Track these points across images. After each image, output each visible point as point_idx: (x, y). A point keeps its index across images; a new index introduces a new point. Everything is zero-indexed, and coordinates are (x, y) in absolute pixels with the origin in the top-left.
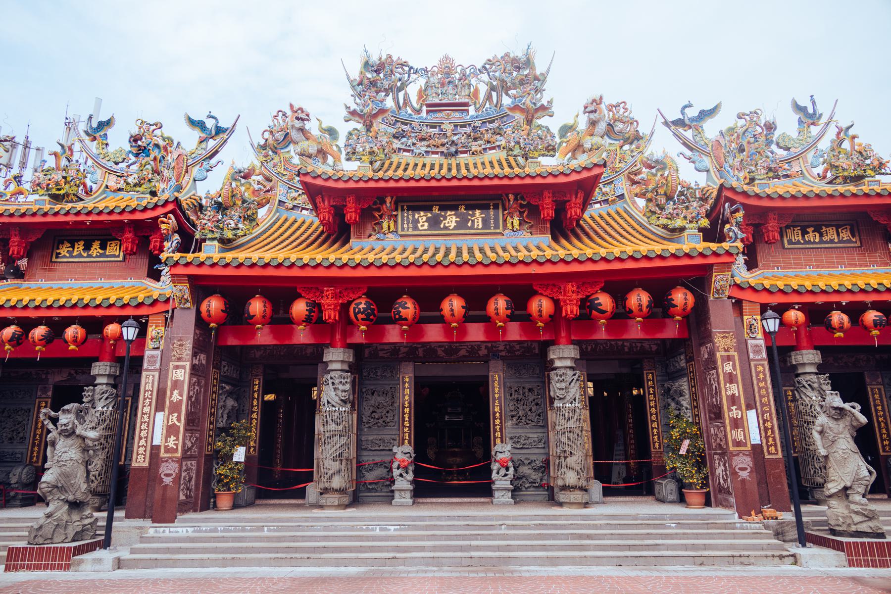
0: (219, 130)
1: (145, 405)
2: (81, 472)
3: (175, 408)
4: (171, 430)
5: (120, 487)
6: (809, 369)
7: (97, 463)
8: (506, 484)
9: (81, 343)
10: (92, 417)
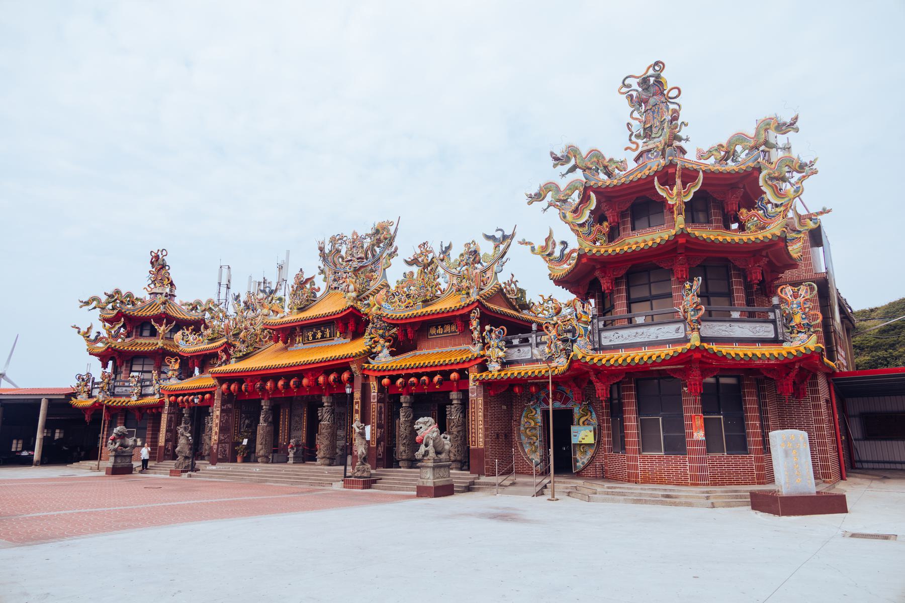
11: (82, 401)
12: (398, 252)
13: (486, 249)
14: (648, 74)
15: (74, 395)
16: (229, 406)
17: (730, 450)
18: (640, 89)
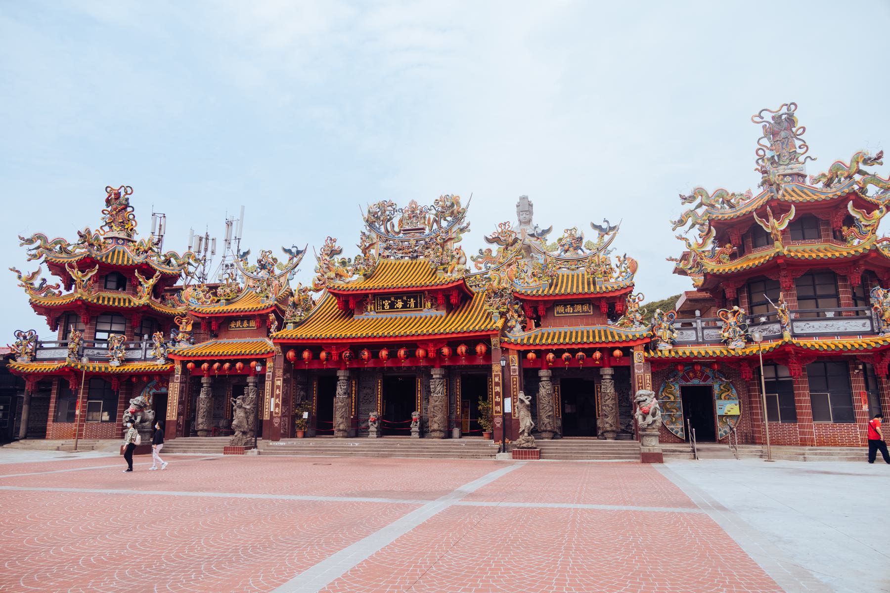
0: (299, 252)
1: (267, 396)
2: (245, 421)
3: (278, 396)
4: (277, 405)
5: (260, 429)
6: (544, 379)
7: (251, 418)
8: (417, 429)
9: (242, 369)
10: (248, 400)
11: (22, 364)
12: (470, 227)
13: (591, 236)
14: (781, 112)
15: (12, 356)
16: (288, 375)
17: (784, 419)
18: (772, 122)
